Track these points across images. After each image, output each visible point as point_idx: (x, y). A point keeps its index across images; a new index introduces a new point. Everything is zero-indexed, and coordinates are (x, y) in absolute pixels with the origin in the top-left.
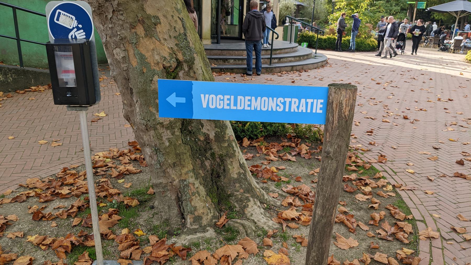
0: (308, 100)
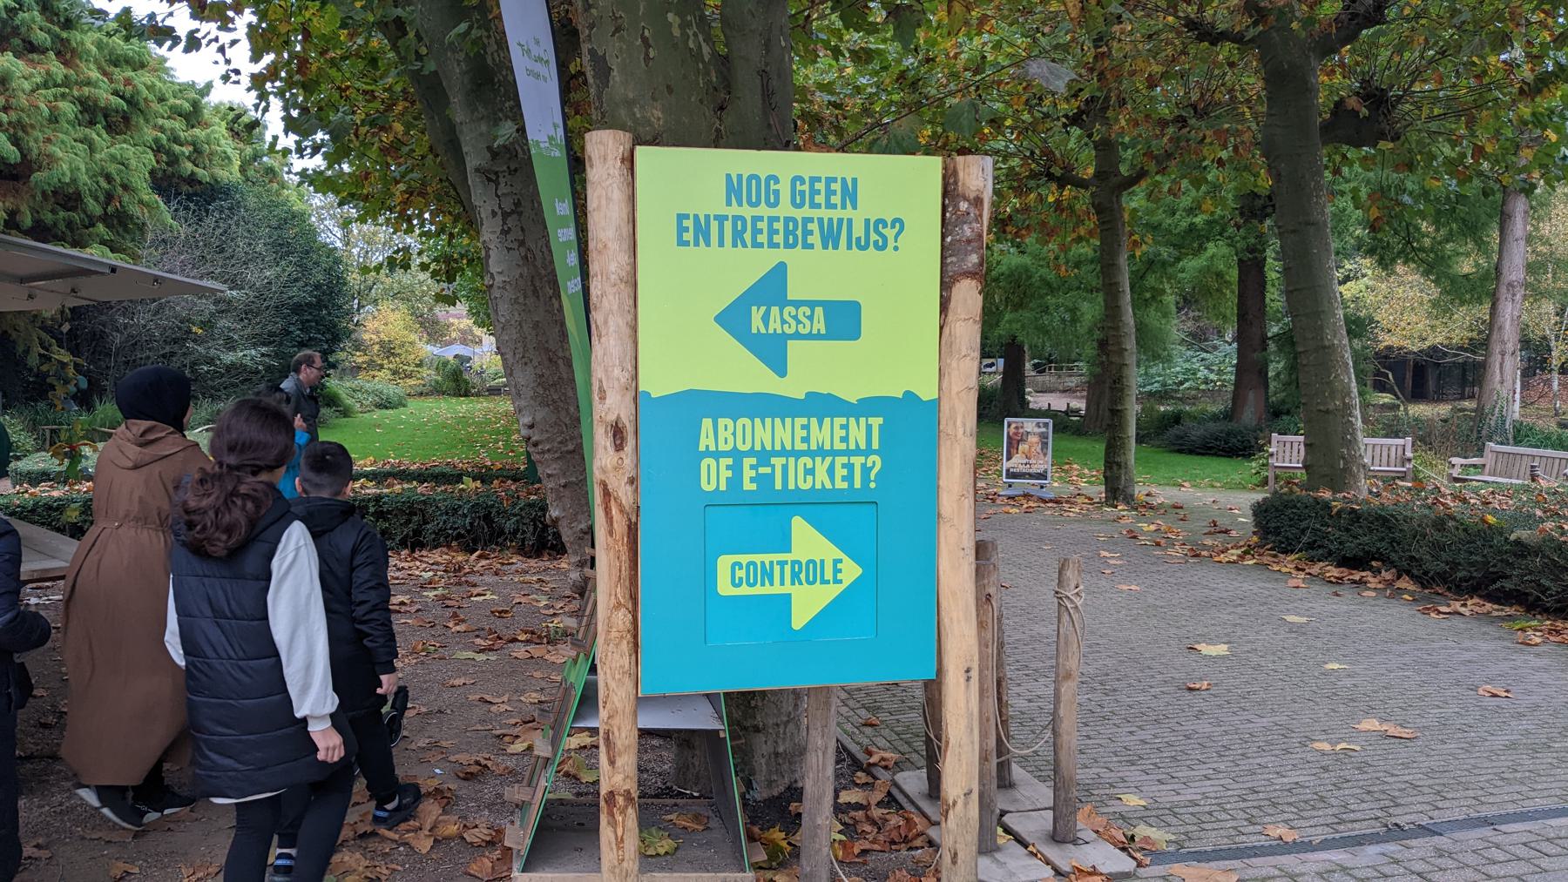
0: (871, 420)
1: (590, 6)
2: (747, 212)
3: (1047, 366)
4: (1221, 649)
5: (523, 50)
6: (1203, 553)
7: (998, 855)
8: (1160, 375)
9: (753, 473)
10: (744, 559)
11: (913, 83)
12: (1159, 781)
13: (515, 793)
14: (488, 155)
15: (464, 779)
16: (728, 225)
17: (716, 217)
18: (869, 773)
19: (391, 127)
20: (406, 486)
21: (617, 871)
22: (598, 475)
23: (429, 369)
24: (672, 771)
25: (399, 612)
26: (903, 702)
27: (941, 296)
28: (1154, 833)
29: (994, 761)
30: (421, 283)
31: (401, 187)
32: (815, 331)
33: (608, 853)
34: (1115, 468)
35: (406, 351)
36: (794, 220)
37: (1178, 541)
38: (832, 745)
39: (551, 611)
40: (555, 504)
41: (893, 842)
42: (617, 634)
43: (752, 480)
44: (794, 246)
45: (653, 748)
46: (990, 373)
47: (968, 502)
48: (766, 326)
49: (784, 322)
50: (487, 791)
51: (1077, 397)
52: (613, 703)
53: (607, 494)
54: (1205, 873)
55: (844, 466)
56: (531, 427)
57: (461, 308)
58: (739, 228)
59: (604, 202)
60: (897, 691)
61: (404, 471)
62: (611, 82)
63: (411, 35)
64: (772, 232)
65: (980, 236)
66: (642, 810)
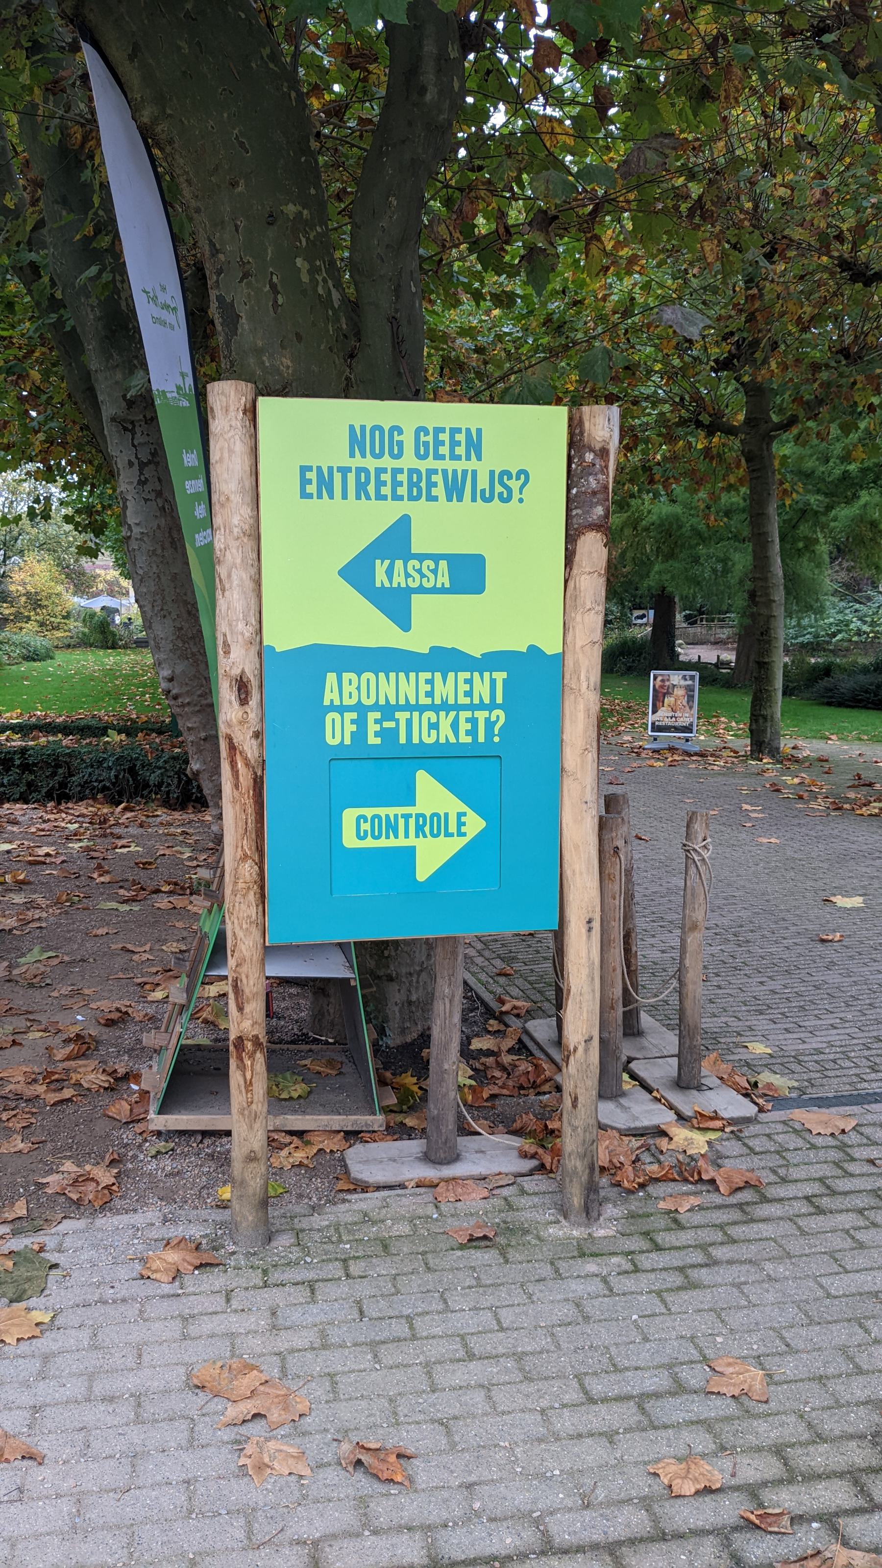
0: (495, 675)
1: (218, 251)
2: (371, 464)
3: (699, 618)
4: (856, 901)
5: (149, 297)
6: (845, 806)
7: (623, 1101)
8: (812, 627)
9: (377, 727)
10: (369, 812)
11: (559, 327)
12: (786, 1029)
13: (150, 1039)
14: (124, 404)
15: (106, 1025)
16: (351, 477)
17: (340, 469)
18: (501, 1021)
19: (28, 375)
20: (51, 738)
21: (246, 1112)
22: (223, 729)
23: (76, 621)
24: (308, 1019)
25: (44, 863)
26: (538, 952)
27: (566, 549)
28: (777, 1080)
29: (620, 1010)
30: (66, 533)
31: (41, 436)
32: (439, 585)
33: (237, 1097)
34: (761, 721)
35: (53, 603)
36: (418, 472)
37: (821, 794)
38: (460, 991)
39: (195, 863)
40: (196, 757)
41: (521, 1087)
42: (244, 885)
43: (377, 734)
44: (418, 498)
45: (291, 996)
46: (641, 625)
47: (592, 756)
48: (391, 580)
49: (407, 575)
50: (127, 1036)
51: (728, 649)
52: (241, 951)
53: (232, 748)
54: (824, 1118)
55: (468, 720)
56: (171, 680)
57: (106, 558)
58: (363, 480)
59: (226, 455)
60: (532, 942)
61: (50, 724)
62: (240, 330)
63: (46, 279)
64: (396, 484)
65: (606, 488)
66: (271, 1055)
